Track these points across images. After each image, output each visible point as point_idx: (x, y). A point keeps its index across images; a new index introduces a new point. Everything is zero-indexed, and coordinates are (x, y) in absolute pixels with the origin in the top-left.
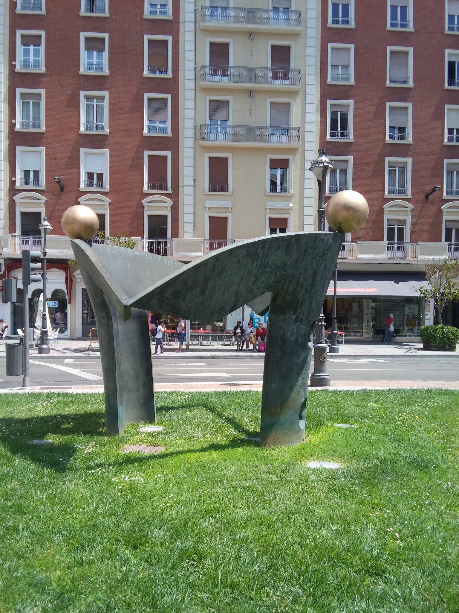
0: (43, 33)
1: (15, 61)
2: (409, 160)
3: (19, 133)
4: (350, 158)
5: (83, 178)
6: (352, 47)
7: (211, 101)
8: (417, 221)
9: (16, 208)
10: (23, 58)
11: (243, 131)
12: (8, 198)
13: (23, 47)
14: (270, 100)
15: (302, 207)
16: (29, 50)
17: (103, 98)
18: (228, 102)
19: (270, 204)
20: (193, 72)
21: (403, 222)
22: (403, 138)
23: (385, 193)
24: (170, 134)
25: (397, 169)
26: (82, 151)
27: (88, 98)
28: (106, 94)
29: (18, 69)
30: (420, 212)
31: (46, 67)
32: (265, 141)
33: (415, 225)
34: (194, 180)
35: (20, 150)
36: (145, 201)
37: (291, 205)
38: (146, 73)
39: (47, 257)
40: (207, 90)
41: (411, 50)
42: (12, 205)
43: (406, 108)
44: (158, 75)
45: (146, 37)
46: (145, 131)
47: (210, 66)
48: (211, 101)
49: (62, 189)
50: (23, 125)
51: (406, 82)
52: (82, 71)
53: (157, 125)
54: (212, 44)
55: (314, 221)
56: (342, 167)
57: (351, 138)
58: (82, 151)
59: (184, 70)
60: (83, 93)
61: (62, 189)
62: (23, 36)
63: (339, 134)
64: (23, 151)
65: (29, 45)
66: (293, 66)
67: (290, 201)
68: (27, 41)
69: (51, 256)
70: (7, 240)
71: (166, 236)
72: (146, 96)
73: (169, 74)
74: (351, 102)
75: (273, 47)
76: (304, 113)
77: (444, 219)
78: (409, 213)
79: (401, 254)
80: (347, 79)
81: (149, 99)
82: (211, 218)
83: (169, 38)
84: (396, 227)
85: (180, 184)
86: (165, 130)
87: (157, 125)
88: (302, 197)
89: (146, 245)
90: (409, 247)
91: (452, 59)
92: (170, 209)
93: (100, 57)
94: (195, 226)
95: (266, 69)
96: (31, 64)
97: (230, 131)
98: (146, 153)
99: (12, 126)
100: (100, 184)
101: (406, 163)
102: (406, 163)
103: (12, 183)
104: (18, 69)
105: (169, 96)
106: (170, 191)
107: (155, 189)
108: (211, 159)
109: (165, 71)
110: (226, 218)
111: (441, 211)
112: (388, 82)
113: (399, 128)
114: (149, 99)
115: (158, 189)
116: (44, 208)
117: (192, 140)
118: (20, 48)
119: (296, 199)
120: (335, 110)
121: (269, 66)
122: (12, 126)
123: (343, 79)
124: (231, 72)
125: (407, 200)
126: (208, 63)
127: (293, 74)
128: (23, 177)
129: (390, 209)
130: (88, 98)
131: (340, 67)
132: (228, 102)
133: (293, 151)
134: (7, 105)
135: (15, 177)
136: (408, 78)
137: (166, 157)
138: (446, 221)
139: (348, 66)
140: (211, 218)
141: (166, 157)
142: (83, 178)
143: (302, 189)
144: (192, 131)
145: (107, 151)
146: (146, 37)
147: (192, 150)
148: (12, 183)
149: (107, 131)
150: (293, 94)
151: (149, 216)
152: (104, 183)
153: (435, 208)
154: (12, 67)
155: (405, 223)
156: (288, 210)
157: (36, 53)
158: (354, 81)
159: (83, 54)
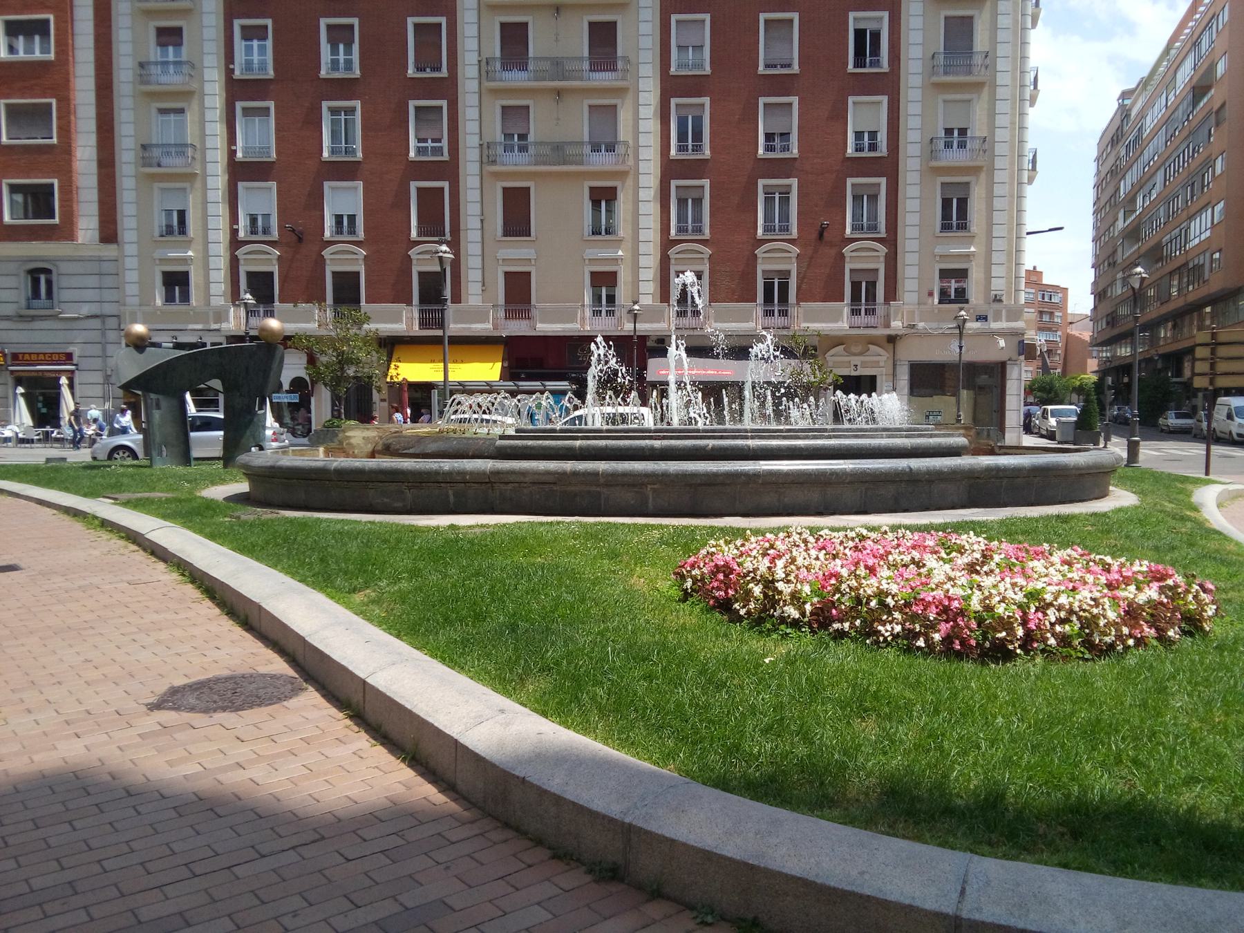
0: (269, 22)
1: (233, 64)
2: (794, 182)
3: (242, 163)
4: (706, 183)
5: (329, 223)
6: (707, 17)
7: (504, 108)
8: (805, 271)
9: (240, 267)
10: (244, 58)
11: (546, 150)
12: (228, 254)
13: (244, 43)
14: (587, 102)
15: (636, 255)
16: (252, 46)
17: (353, 110)
18: (528, 107)
19: (591, 253)
20: (477, 67)
21: (785, 274)
22: (786, 149)
23: (759, 231)
24: (446, 157)
25: (777, 196)
26: (327, 185)
27: (334, 111)
28: (357, 104)
29: (237, 74)
30: (811, 258)
31: (275, 70)
32: (581, 163)
33: (804, 278)
34: (482, 221)
35: (329, 187)
36: (326, 253)
37: (620, 253)
38: (411, 72)
39: (637, 334)
40: (496, 92)
41: (795, 16)
42: (234, 263)
43: (790, 105)
44: (428, 74)
45: (411, 21)
46: (412, 154)
47: (502, 59)
48: (504, 108)
49: (300, 240)
50: (333, 151)
51: (789, 66)
52: (323, 73)
53: (430, 144)
54: (504, 26)
55: (655, 275)
56: (871, 193)
57: (707, 153)
58: (327, 185)
59: (75, 77)
60: (325, 105)
61: (300, 240)
62: (243, 28)
63: (690, 147)
64: (247, 188)
65: (251, 40)
66: (620, 53)
67: (619, 248)
68: (250, 34)
69: (397, 332)
70: (227, 312)
71: (357, 301)
72: (412, 104)
73: (444, 73)
74: (706, 100)
75: (591, 24)
76: (636, 119)
77: (848, 267)
78: (794, 260)
79: (871, 320)
80: (701, 66)
81: (417, 109)
82: (506, 273)
83: (443, 20)
84: (776, 281)
85: (462, 226)
86: (438, 151)
87: (430, 144)
88: (636, 241)
89: (416, 315)
90: (793, 311)
91: (861, 26)
92: (882, 259)
93: (348, 51)
94: (483, 285)
95: (581, 59)
96: (256, 66)
97: (532, 150)
98: (414, 186)
99: (232, 153)
100: (352, 231)
101: (790, 186)
102: (790, 186)
103: (234, 232)
104: (237, 74)
105: (444, 103)
106: (883, 235)
107: (424, 236)
108: (505, 190)
109: (439, 69)
110: (529, 273)
111: (842, 257)
112: (761, 68)
113: (782, 134)
114: (417, 109)
115: (428, 236)
116: (277, 267)
117: (478, 164)
118: (239, 44)
119: (628, 244)
120: (683, 113)
121: (586, 53)
122: (232, 153)
123: (695, 66)
124: (531, 67)
125: (704, 242)
126: (498, 54)
127: (620, 65)
128: (248, 224)
129: (332, 257)
130: (334, 111)
131: (691, 49)
132: (528, 107)
133: (622, 175)
134: (225, 126)
135: (238, 224)
136: (792, 59)
137: (442, 189)
138: (851, 270)
139: (702, 46)
140: (506, 273)
141: (442, 189)
142: (329, 223)
143: (636, 229)
144: (477, 151)
145: (360, 184)
146: (411, 21)
147: (478, 178)
148: (234, 232)
149: (360, 155)
150: (620, 92)
151: (420, 274)
152: (356, 230)
153: (833, 252)
154: (229, 72)
155: (790, 275)
156: (615, 260)
157: (262, 50)
158: (709, 69)
159: (325, 49)
